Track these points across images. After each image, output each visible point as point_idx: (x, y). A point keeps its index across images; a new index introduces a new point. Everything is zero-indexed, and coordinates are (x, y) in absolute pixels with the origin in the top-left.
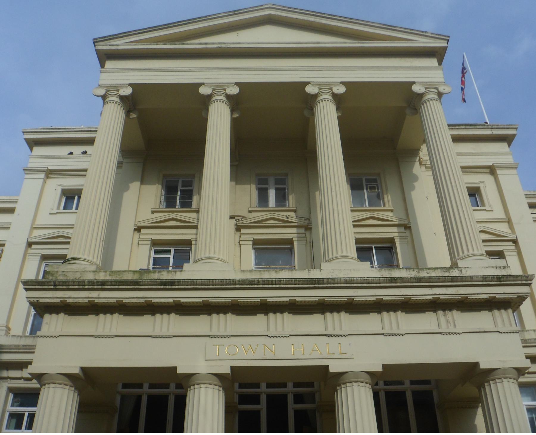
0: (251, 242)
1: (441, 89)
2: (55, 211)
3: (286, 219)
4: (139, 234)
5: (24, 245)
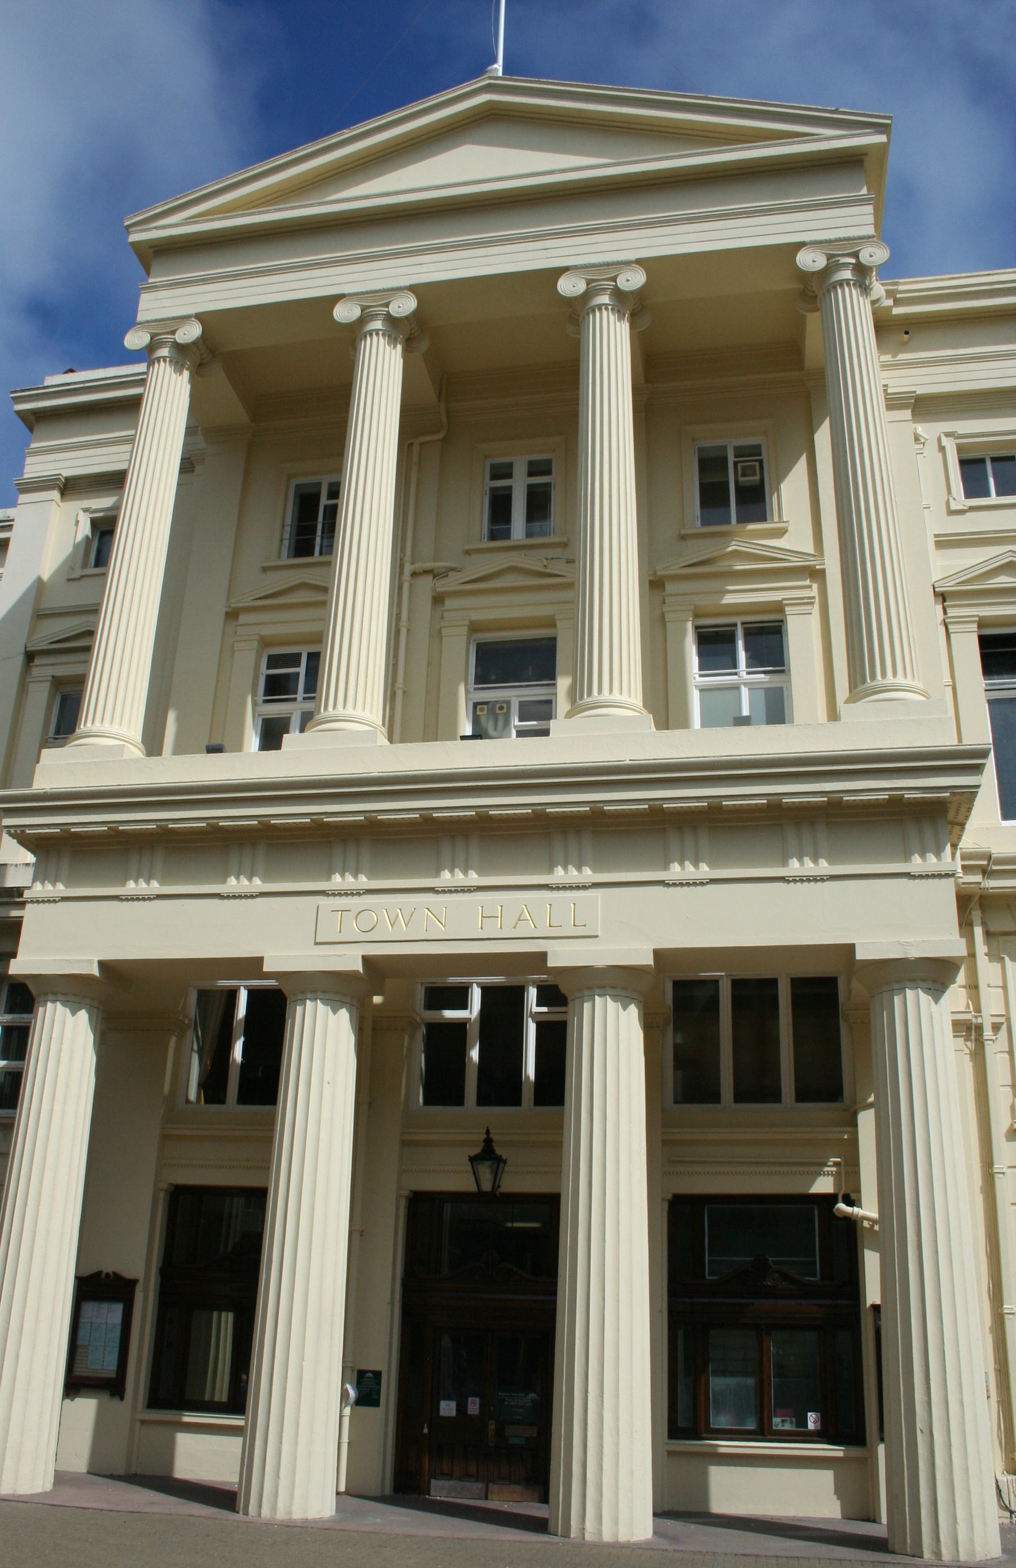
0: (464, 630)
1: (864, 257)
2: (77, 574)
3: (543, 570)
4: (236, 625)
5: (19, 660)
